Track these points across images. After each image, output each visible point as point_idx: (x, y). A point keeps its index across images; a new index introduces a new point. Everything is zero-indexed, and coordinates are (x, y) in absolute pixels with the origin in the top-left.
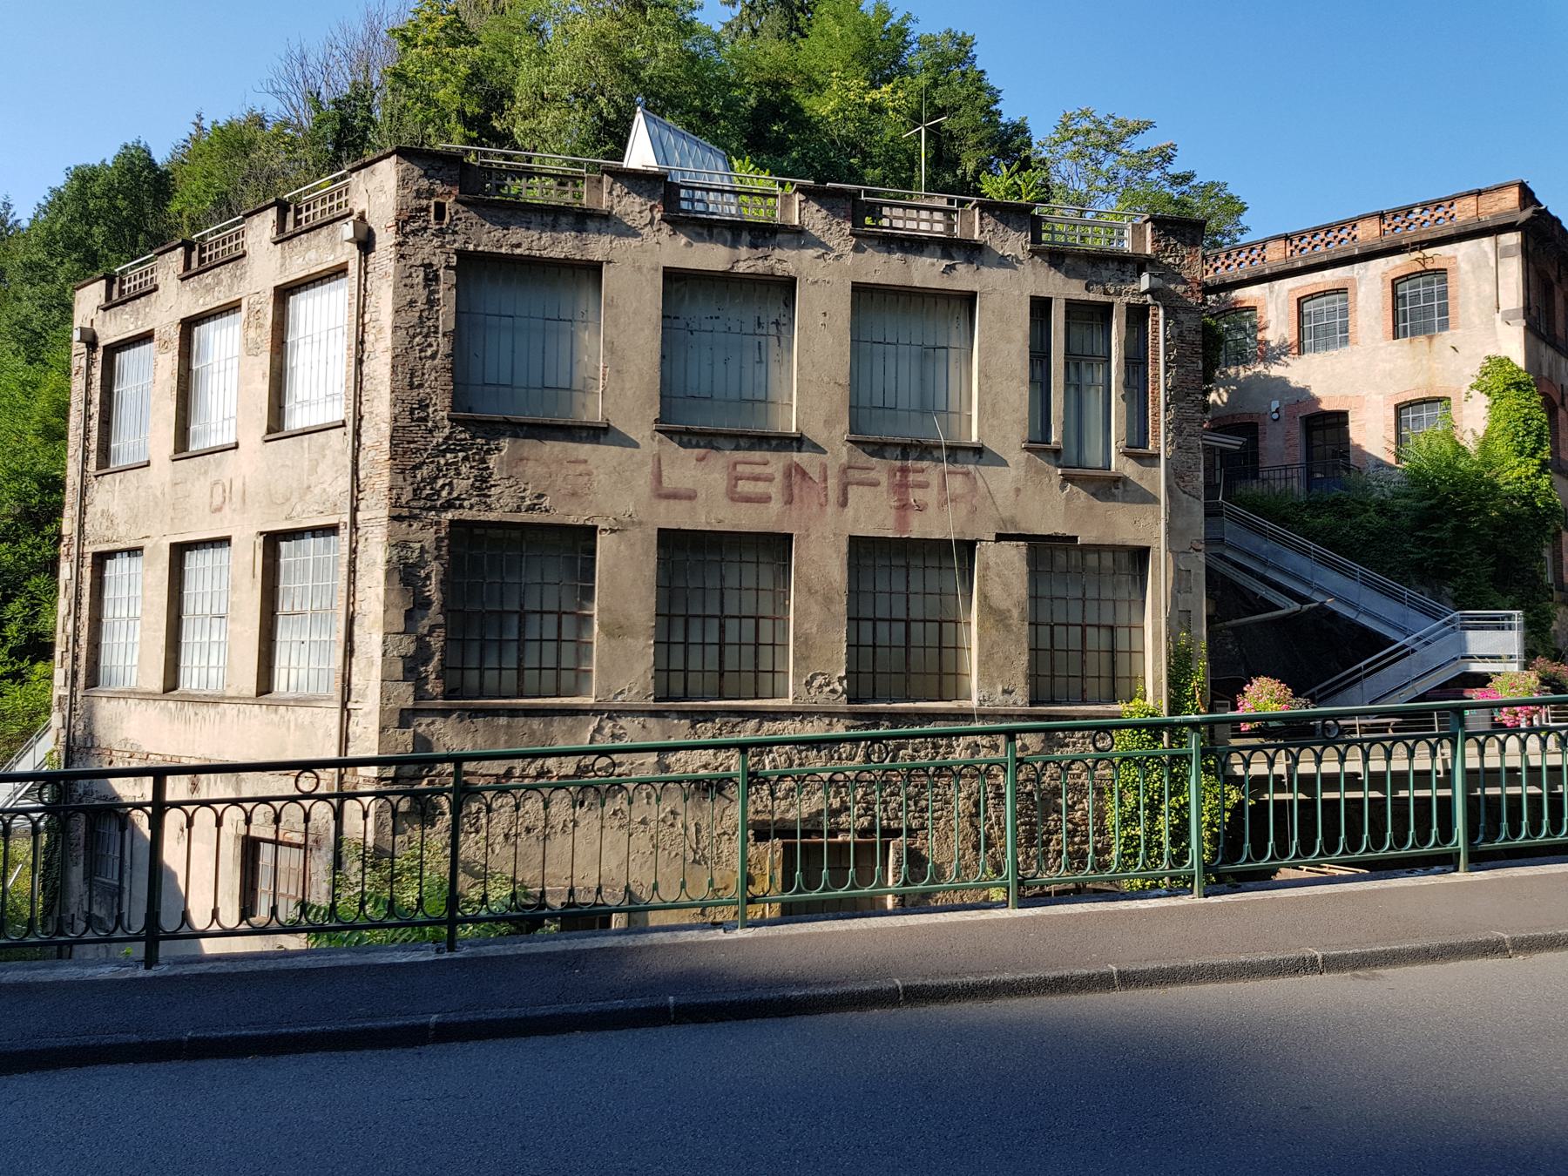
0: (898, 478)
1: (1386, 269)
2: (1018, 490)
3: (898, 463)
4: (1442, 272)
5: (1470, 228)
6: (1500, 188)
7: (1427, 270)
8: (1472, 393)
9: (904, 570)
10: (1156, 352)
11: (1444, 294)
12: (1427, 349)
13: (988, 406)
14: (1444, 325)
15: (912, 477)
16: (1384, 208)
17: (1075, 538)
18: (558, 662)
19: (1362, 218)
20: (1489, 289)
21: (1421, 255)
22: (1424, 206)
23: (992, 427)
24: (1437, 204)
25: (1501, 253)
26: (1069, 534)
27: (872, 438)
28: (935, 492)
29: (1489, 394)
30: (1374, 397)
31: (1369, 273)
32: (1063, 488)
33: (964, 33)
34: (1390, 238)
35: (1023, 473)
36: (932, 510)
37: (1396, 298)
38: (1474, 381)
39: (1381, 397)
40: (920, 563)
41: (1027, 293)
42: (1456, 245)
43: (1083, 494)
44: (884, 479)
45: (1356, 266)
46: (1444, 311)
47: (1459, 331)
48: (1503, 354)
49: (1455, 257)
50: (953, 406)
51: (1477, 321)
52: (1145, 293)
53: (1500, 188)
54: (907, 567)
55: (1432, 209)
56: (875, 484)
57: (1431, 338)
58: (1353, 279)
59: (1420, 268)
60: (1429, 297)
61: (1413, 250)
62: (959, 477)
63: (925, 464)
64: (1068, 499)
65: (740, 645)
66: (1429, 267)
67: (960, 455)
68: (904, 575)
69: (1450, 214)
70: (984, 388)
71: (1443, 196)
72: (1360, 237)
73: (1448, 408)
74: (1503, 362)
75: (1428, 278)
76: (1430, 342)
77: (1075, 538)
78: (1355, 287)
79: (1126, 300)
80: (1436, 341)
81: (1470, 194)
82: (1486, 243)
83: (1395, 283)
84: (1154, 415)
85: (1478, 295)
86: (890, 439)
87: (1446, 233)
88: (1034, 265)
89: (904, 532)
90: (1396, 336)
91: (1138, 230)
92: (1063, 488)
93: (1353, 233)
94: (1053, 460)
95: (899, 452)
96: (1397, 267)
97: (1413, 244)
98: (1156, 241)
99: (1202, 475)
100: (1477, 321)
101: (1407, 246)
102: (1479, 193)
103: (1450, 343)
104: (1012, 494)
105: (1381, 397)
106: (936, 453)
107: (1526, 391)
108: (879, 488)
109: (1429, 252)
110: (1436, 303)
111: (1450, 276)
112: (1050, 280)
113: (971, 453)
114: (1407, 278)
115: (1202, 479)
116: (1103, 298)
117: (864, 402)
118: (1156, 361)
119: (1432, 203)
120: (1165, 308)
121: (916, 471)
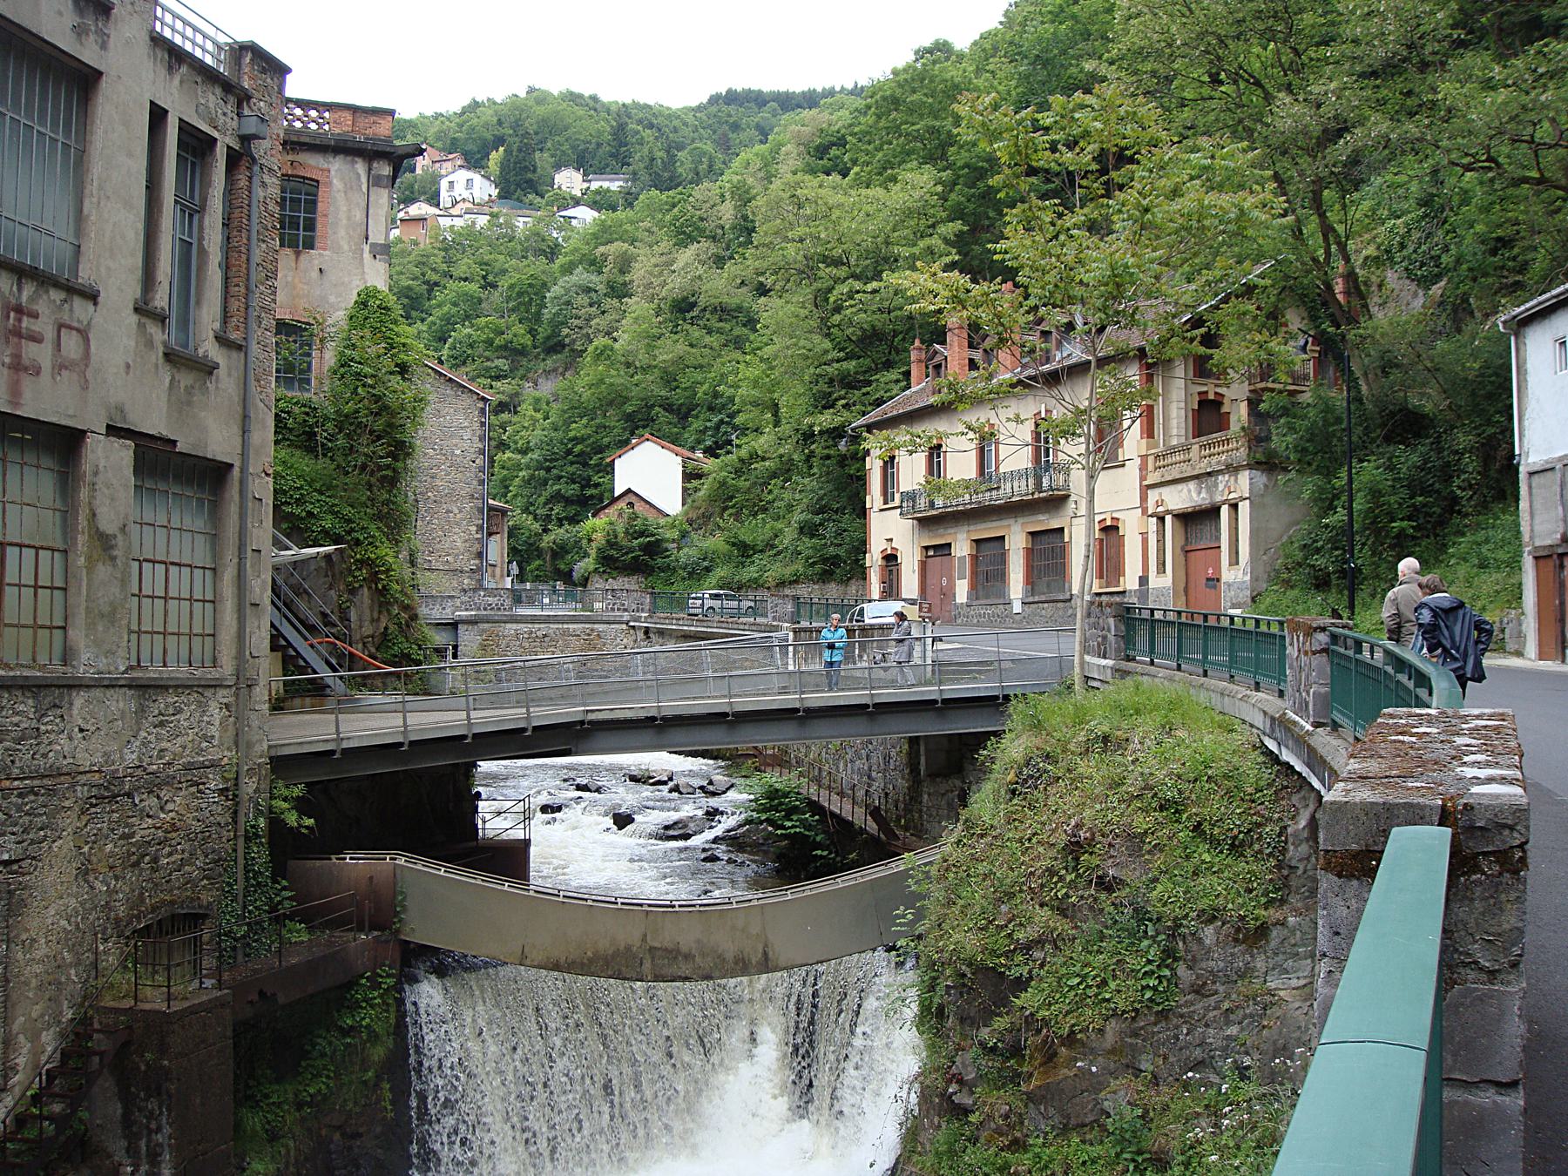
2: (128, 366)
5: (350, 145)
12: (293, 265)
14: (310, 244)
17: (174, 442)
18: (35, 634)
20: (359, 215)
33: (1001, 23)
46: (310, 226)
47: (327, 253)
51: (346, 247)
57: (298, 254)
65: (165, 598)
80: (303, 257)
85: (349, 219)
100: (346, 247)
103: (317, 264)
104: (122, 371)
111: (322, 189)
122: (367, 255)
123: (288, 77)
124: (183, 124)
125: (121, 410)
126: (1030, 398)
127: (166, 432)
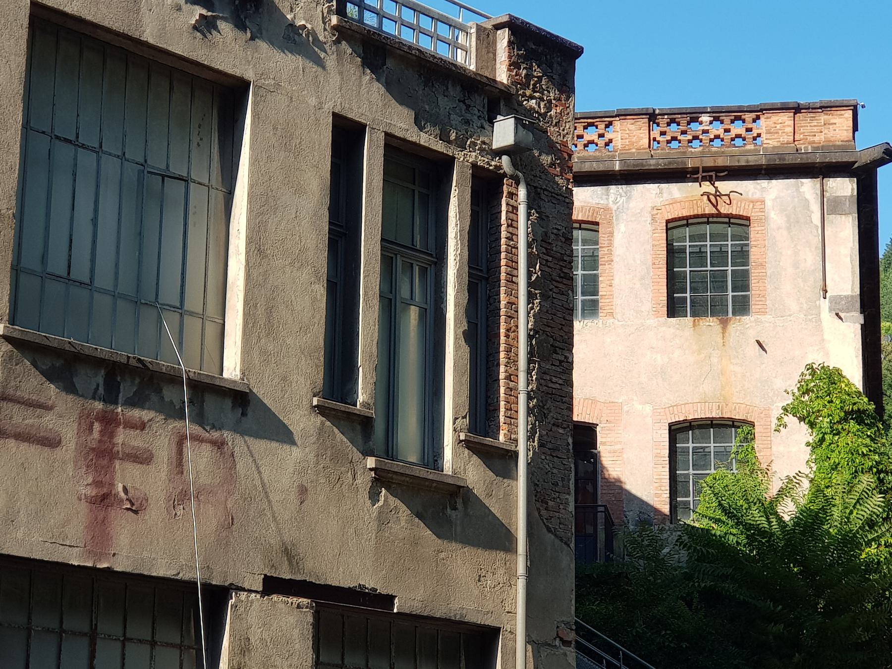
0: (96, 434)
1: (659, 202)
2: (303, 491)
3: (99, 406)
4: (741, 222)
5: (789, 160)
6: (826, 107)
7: (719, 215)
8: (786, 419)
9: (85, 641)
10: (513, 263)
11: (742, 255)
12: (720, 340)
13: (261, 311)
14: (742, 307)
15: (122, 437)
16: (658, 106)
17: (391, 598)
19: (623, 115)
20: (811, 259)
21: (711, 190)
22: (717, 115)
23: (264, 352)
24: (737, 114)
25: (828, 206)
26: (382, 590)
27: (55, 339)
28: (163, 475)
29: (812, 425)
30: (639, 407)
31: (632, 204)
32: (374, 497)
34: (659, 158)
35: (311, 456)
36: (156, 512)
37: (673, 254)
38: (789, 400)
39: (648, 409)
40: (117, 631)
41: (329, 107)
42: (764, 183)
43: (404, 512)
44: (69, 432)
45: (613, 189)
46: (742, 282)
47: (767, 317)
48: (832, 364)
49: (763, 202)
50: (193, 302)
51: (794, 306)
52: (500, 153)
53: (826, 107)
54: (92, 637)
55: (727, 120)
56: (51, 442)
57: (724, 323)
58: (607, 209)
59: (709, 210)
60: (720, 256)
61: (704, 179)
62: (206, 449)
63: (146, 415)
64: (382, 520)
66: (724, 209)
67: (211, 404)
68: (85, 653)
69: (755, 133)
70: (255, 273)
71: (745, 103)
72: (618, 143)
73: (749, 438)
74: (833, 377)
75: (719, 228)
76: (724, 328)
77: (391, 598)
78: (610, 223)
79: (472, 157)
81: (784, 108)
82: (808, 187)
83: (672, 225)
84: (508, 378)
85: (796, 265)
86: (89, 347)
87: (753, 160)
88: (340, 55)
89: (100, 556)
90: (674, 309)
91: (485, 37)
92: (374, 497)
93: (608, 136)
94: (359, 439)
95: (100, 380)
96: (674, 202)
97: (706, 169)
98: (513, 65)
99: (571, 499)
100: (794, 306)
101: (695, 171)
102: (797, 109)
103: (753, 334)
104: (293, 496)
105: (648, 409)
106: (169, 393)
107: (870, 426)
108: (59, 453)
109: (724, 186)
110: (688, 269)
111: (754, 232)
112: (364, 90)
113: (228, 403)
114: (687, 221)
115: (571, 507)
116: (439, 146)
117: (31, 261)
118: (512, 279)
119: (729, 111)
120: (528, 185)
121: (131, 425)
122: (827, 316)
123: (578, 62)
124: (395, 143)
125: (289, 554)
126: (728, 327)
127: (371, 581)
